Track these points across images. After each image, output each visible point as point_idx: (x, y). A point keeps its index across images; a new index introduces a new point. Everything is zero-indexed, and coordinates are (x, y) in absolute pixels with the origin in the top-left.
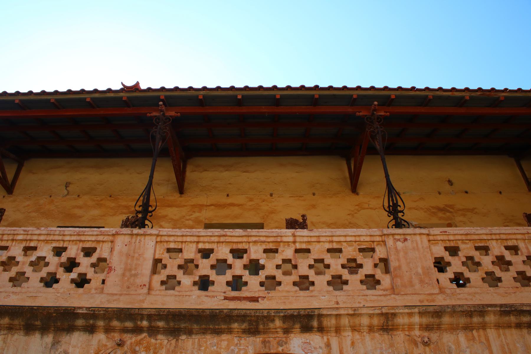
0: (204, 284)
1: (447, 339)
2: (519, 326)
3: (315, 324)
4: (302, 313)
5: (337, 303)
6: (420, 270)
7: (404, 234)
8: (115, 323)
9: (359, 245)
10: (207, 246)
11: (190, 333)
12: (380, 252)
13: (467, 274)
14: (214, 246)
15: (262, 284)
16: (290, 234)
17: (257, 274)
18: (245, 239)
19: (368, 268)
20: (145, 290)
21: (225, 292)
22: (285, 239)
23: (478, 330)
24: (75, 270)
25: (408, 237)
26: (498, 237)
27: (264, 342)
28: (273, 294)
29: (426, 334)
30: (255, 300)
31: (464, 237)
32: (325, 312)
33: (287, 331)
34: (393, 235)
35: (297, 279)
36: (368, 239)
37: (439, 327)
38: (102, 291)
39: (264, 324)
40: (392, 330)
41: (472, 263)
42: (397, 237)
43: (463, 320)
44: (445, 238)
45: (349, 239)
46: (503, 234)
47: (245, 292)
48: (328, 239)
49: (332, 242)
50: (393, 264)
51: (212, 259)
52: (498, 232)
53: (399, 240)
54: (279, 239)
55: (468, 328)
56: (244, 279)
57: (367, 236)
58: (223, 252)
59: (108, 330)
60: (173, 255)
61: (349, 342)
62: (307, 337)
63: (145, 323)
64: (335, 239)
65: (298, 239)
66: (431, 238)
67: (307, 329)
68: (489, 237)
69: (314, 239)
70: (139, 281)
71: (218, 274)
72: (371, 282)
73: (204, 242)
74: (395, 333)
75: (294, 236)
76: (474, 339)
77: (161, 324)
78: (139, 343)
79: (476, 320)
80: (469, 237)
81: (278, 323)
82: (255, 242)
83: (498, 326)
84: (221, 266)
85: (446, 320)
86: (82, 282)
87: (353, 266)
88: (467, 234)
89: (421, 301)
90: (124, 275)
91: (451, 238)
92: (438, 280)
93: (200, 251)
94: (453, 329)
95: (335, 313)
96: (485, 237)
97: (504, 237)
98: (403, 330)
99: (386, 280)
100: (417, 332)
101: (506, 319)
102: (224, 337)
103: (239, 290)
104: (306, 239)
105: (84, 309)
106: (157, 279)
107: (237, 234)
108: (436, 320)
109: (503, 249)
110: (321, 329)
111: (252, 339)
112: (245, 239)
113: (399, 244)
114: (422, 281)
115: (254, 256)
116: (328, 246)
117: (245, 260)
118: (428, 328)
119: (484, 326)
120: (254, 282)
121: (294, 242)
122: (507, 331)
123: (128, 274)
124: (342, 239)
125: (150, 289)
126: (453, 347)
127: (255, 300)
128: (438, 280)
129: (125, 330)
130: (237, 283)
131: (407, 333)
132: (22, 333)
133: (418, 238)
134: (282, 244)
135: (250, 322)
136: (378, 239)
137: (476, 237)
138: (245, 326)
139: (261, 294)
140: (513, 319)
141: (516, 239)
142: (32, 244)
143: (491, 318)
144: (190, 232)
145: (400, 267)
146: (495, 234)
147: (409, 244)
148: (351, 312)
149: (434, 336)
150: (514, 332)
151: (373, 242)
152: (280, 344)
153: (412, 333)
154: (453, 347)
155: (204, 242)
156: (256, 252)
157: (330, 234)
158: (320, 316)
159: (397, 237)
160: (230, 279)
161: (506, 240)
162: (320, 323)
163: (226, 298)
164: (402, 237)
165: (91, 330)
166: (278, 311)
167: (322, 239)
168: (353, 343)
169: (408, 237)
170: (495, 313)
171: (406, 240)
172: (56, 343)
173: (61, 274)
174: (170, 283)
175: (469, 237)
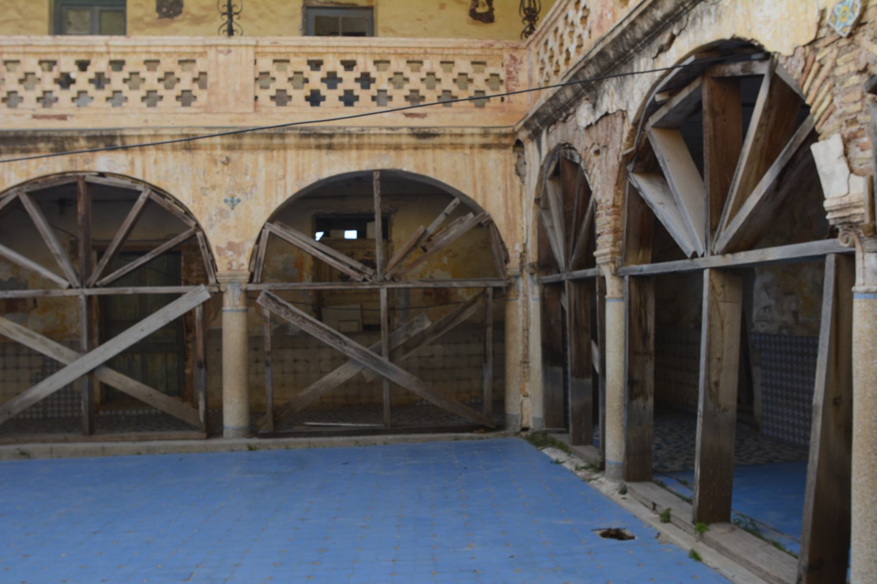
0: (315, 99)
1: (247, 158)
2: (319, 147)
3: (119, 143)
4: (104, 133)
5: (146, 121)
6: (238, 88)
7: (229, 46)
9: (179, 56)
10: (119, 57)
12: (201, 65)
13: (291, 91)
15: (374, 98)
16: (102, 43)
17: (346, 92)
18: (53, 50)
19: (186, 83)
21: (34, 110)
22: (98, 49)
23: (279, 149)
25: (233, 49)
26: (335, 50)
27: (71, 161)
28: (83, 111)
29: (227, 153)
30: (63, 118)
31: (296, 50)
32: (126, 133)
34: (216, 46)
35: (110, 94)
36: (189, 50)
37: (240, 147)
39: (69, 144)
40: (194, 149)
41: (168, 79)
42: (220, 48)
43: (263, 142)
44: (275, 50)
45: (167, 49)
46: (343, 47)
47: (55, 110)
48: (145, 49)
49: (148, 52)
50: (211, 79)
51: (91, 73)
52: (336, 44)
53: (222, 52)
54: (90, 50)
55: (269, 148)
56: (55, 95)
57: (187, 46)
58: (332, 64)
60: (187, 65)
61: (152, 160)
62: (112, 154)
64: (153, 49)
65: (112, 49)
66: (259, 50)
67: (111, 148)
68: (325, 50)
69: (129, 50)
72: (186, 98)
73: (9, 53)
74: (198, 152)
75: (107, 45)
76: (272, 159)
79: (276, 141)
80: (303, 50)
81: (83, 143)
82: (65, 53)
83: (298, 147)
84: (332, 80)
85: (247, 141)
87: (168, 79)
88: (300, 47)
89: (231, 121)
91: (282, 50)
92: (256, 98)
93: (112, 63)
94: (254, 149)
95: (136, 133)
96: (321, 50)
97: (342, 50)
98: (206, 149)
99: (203, 97)
100: (219, 152)
101: (306, 141)
104: (120, 50)
107: (43, 43)
108: (236, 141)
109: (338, 63)
110: (125, 148)
111: (59, 158)
112: (53, 50)
113: (222, 57)
114: (237, 100)
115: (64, 69)
116: (146, 57)
118: (230, 148)
119: (285, 147)
120: (65, 96)
121: (108, 53)
122: (307, 152)
124: (160, 50)
126: (251, 166)
127: (63, 118)
128: (256, 98)
130: (45, 99)
131: (209, 152)
133: (243, 49)
134: (95, 55)
135: (55, 142)
136: (200, 50)
137: (311, 50)
138: (51, 145)
139: (71, 112)
140: (312, 141)
141: (357, 53)
143: (291, 140)
144: (431, 43)
145: (216, 83)
146: (333, 47)
147: (232, 57)
148: (152, 132)
149: (234, 156)
150: (314, 153)
151: (195, 53)
152: (86, 162)
153: (214, 153)
154: (251, 166)
155: (9, 53)
156: (365, 64)
157: (145, 43)
158: (122, 137)
159: (220, 48)
161: (345, 53)
162: (123, 143)
163: (35, 117)
164: (227, 48)
166: (81, 131)
167: (139, 49)
168: (156, 162)
169: (233, 49)
170: (295, 135)
171: (229, 52)
175: (303, 50)
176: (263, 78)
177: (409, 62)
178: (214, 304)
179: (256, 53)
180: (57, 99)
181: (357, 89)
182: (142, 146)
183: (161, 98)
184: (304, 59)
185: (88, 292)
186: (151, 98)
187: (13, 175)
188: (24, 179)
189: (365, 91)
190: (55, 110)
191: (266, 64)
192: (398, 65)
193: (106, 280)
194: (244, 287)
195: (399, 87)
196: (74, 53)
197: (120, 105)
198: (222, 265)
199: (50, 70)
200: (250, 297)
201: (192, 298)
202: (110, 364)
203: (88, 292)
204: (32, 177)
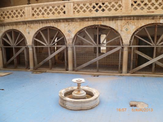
8: (126, 18)
11: (141, 19)
14: (98, 2)
20: (130, 11)
24: (114, 7)
33: (160, 19)
38: (121, 12)
47: (151, 10)
59: (125, 19)
63: (132, 18)
70: (129, 9)
71: (116, 4)
77: (135, 18)
78: (131, 22)
86: (116, 10)
90: (125, 8)
93: (141, 1)
102: (147, 20)
103: (150, 10)
105: (139, 29)
106: (133, 8)
115: (153, 2)
117: (151, 3)
120: (153, 8)
123: (126, 8)
125: (131, 11)
129: (128, 19)
132: (108, 21)
142: (91, 3)
160: (148, 7)
163: (147, 12)
165: (121, 20)
172: (115, 23)
173: (112, 8)
174: (135, 9)
176: (75, 8)
177: (115, 2)
178: (67, 48)
179: (74, 4)
180: (92, 11)
181: (105, 8)
182: (91, 18)
183: (118, 9)
184: (101, 3)
185: (156, 46)
186: (97, 11)
187: (143, 24)
188: (145, 24)
189: (85, 9)
190: (151, 10)
191: (76, 5)
192: (51, 7)
193: (91, 43)
194: (128, 46)
195: (40, 12)
196: (36, 7)
197: (136, 10)
198: (68, 42)
199: (117, 4)
200: (72, 48)
201: (119, 48)
202: (148, 61)
203: (156, 46)
204: (147, 24)
